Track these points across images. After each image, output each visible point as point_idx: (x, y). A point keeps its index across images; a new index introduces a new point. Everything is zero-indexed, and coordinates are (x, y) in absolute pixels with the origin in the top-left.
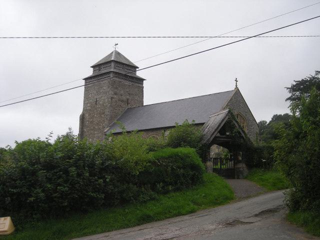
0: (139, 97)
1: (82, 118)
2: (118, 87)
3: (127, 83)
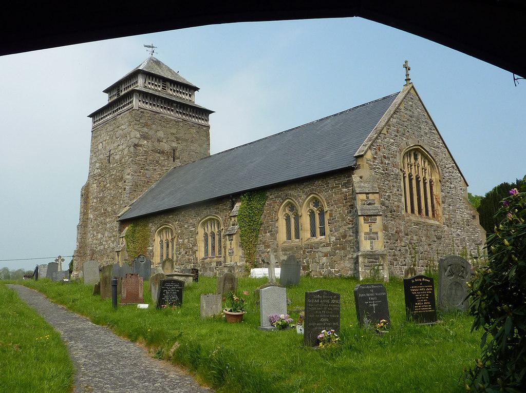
0: (201, 146)
2: (149, 123)
3: (172, 115)
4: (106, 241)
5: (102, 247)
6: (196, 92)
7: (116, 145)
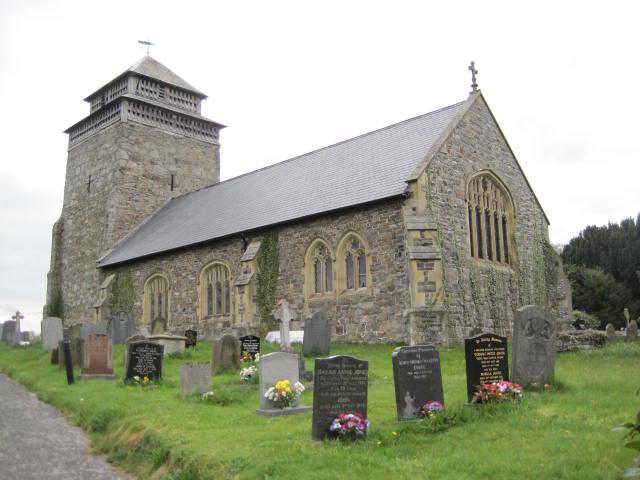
1: (59, 232)
2: (141, 140)
3: (170, 131)
4: (84, 295)
5: (78, 302)
6: (203, 101)
7: (97, 168)
